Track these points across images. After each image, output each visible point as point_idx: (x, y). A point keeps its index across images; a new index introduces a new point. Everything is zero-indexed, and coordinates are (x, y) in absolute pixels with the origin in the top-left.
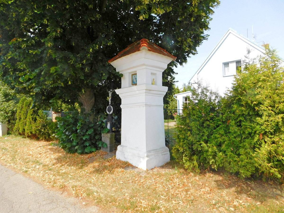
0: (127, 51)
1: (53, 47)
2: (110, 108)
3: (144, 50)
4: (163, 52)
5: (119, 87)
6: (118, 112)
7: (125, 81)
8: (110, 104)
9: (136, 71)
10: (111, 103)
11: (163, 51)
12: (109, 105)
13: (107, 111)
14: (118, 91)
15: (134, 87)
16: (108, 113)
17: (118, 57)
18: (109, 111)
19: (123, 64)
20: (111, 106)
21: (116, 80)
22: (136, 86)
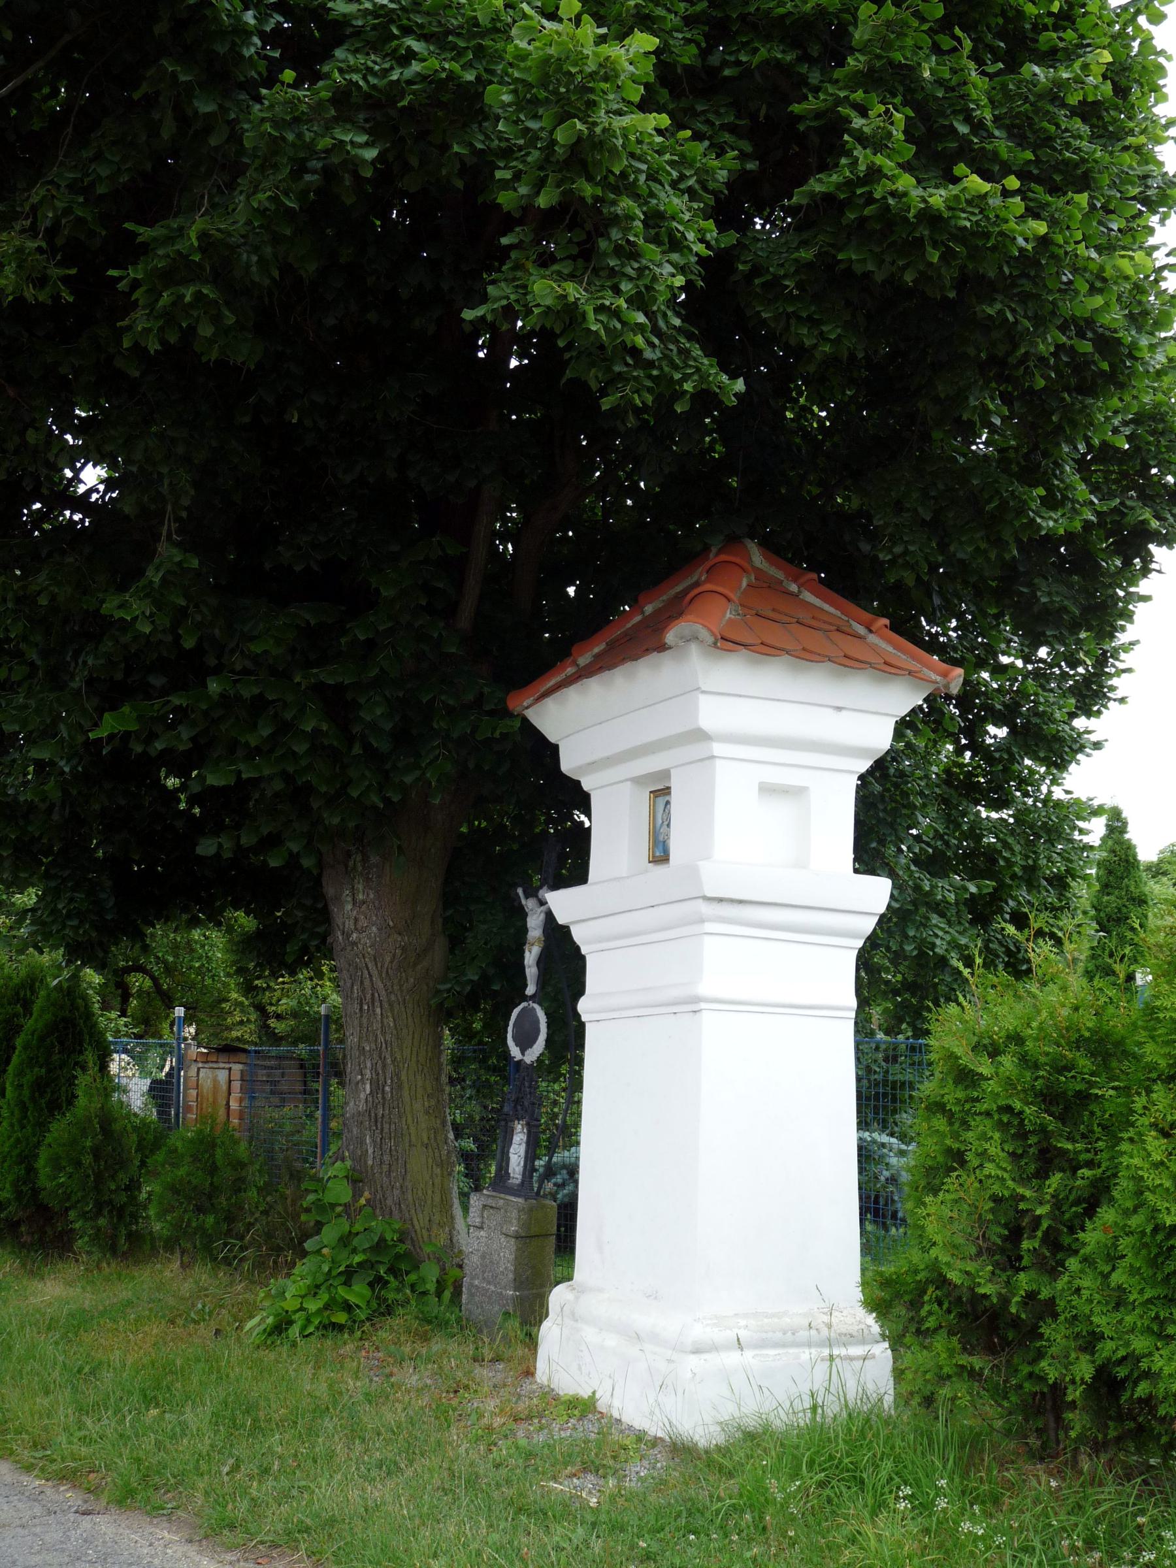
0: (625, 634)
1: (602, 235)
2: (528, 1014)
3: (694, 649)
4: (860, 637)
5: (574, 871)
6: (568, 1040)
7: (613, 829)
8: (531, 990)
9: (666, 774)
10: (542, 982)
11: (861, 630)
12: (525, 998)
13: (510, 1042)
14: (564, 904)
15: (660, 870)
16: (515, 1052)
17: (570, 670)
18: (525, 1043)
19: (590, 724)
20: (536, 1006)
21: (545, 826)
22: (1121, 807)
